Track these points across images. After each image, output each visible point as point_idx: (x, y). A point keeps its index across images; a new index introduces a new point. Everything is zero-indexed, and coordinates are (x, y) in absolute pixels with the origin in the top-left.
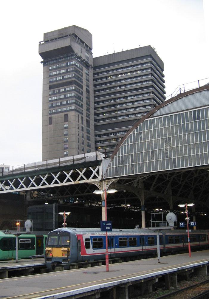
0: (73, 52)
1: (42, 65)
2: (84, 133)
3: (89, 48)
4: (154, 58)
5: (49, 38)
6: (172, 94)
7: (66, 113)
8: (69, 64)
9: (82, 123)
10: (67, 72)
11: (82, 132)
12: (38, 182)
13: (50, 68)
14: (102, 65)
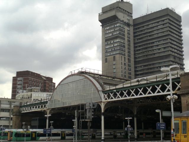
0: (117, 18)
1: (101, 27)
2: (126, 66)
3: (130, 14)
4: (172, 15)
5: (105, 10)
6: (82, 68)
7: (114, 56)
8: (115, 26)
9: (125, 61)
10: (115, 31)
11: (124, 66)
12: (145, 91)
13: (106, 29)
14: (139, 23)
